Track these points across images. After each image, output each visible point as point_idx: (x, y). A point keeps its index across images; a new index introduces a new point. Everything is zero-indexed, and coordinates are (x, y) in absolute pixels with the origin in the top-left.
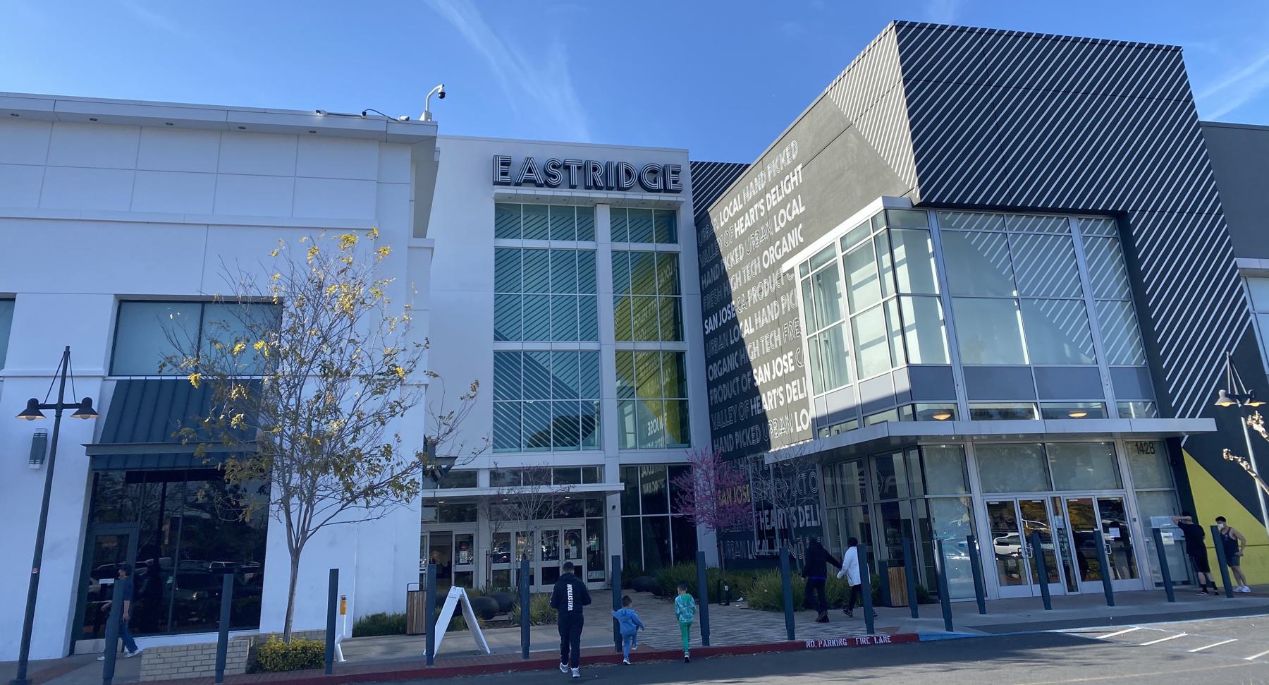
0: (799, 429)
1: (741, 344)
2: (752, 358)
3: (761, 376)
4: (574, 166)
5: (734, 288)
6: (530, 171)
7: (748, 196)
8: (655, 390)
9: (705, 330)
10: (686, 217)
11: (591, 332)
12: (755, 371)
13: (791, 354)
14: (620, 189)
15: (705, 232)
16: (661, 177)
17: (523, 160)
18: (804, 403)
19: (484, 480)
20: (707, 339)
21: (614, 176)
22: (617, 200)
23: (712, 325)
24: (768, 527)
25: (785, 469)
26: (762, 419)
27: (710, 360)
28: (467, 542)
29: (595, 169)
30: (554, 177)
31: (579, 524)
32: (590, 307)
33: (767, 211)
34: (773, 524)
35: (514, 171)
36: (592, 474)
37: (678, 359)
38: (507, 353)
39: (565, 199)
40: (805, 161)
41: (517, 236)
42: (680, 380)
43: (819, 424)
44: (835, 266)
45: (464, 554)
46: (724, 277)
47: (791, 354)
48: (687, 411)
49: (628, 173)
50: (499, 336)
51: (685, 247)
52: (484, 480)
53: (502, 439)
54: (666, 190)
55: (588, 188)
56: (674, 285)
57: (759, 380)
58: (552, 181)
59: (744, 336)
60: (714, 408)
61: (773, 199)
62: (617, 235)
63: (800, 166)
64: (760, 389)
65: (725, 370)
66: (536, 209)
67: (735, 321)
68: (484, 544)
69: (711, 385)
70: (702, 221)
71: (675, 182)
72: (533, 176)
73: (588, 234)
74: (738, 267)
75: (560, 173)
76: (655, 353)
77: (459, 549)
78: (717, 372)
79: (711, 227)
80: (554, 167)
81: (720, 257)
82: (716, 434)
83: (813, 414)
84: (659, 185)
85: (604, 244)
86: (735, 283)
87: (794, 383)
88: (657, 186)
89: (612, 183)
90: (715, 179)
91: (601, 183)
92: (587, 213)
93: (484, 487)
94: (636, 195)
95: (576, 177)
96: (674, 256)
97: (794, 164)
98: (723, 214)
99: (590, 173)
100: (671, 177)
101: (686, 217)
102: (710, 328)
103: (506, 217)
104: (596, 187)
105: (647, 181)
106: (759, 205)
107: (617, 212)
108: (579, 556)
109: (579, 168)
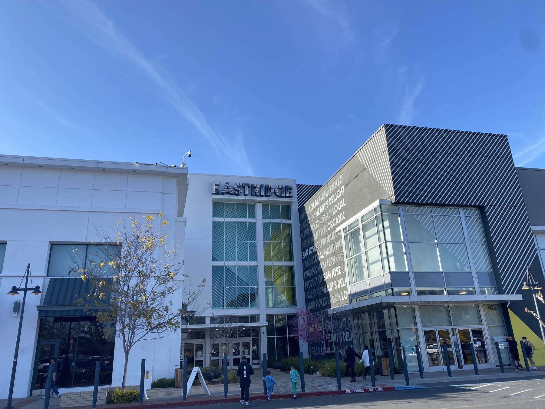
0: (343, 299)
1: (318, 263)
2: (323, 269)
3: (327, 276)
5: (315, 239)
6: (228, 188)
7: (321, 199)
8: (281, 282)
9: (303, 256)
10: (295, 208)
11: (254, 258)
12: (324, 274)
13: (340, 267)
15: (303, 214)
16: (284, 191)
17: (224, 184)
18: (345, 288)
19: (208, 321)
20: (304, 260)
21: (264, 191)
22: (265, 201)
24: (330, 341)
25: (337, 316)
26: (327, 295)
27: (305, 270)
28: (201, 348)
29: (255, 188)
31: (249, 340)
32: (254, 247)
35: (221, 188)
36: (254, 318)
39: (242, 200)
41: (222, 216)
42: (292, 278)
43: (352, 297)
44: (359, 229)
45: (199, 353)
46: (311, 234)
47: (340, 267)
49: (270, 189)
51: (294, 221)
52: (208, 321)
53: (216, 304)
54: (286, 197)
55: (252, 196)
56: (290, 237)
57: (326, 278)
58: (237, 192)
59: (319, 259)
60: (307, 290)
61: (332, 200)
62: (265, 216)
63: (343, 187)
66: (230, 204)
67: (316, 253)
69: (305, 280)
70: (302, 210)
71: (290, 193)
72: (229, 191)
75: (241, 189)
76: (281, 267)
77: (197, 351)
78: (308, 275)
79: (305, 213)
80: (238, 186)
81: (309, 225)
82: (308, 301)
85: (259, 220)
86: (316, 236)
87: (341, 280)
88: (282, 195)
89: (263, 194)
90: (307, 192)
91: (258, 193)
92: (252, 206)
93: (208, 324)
95: (248, 191)
96: (289, 225)
97: (341, 185)
98: (311, 207)
99: (253, 189)
100: (288, 191)
101: (295, 208)
102: (305, 256)
105: (278, 193)
106: (326, 203)
107: (265, 206)
109: (249, 187)
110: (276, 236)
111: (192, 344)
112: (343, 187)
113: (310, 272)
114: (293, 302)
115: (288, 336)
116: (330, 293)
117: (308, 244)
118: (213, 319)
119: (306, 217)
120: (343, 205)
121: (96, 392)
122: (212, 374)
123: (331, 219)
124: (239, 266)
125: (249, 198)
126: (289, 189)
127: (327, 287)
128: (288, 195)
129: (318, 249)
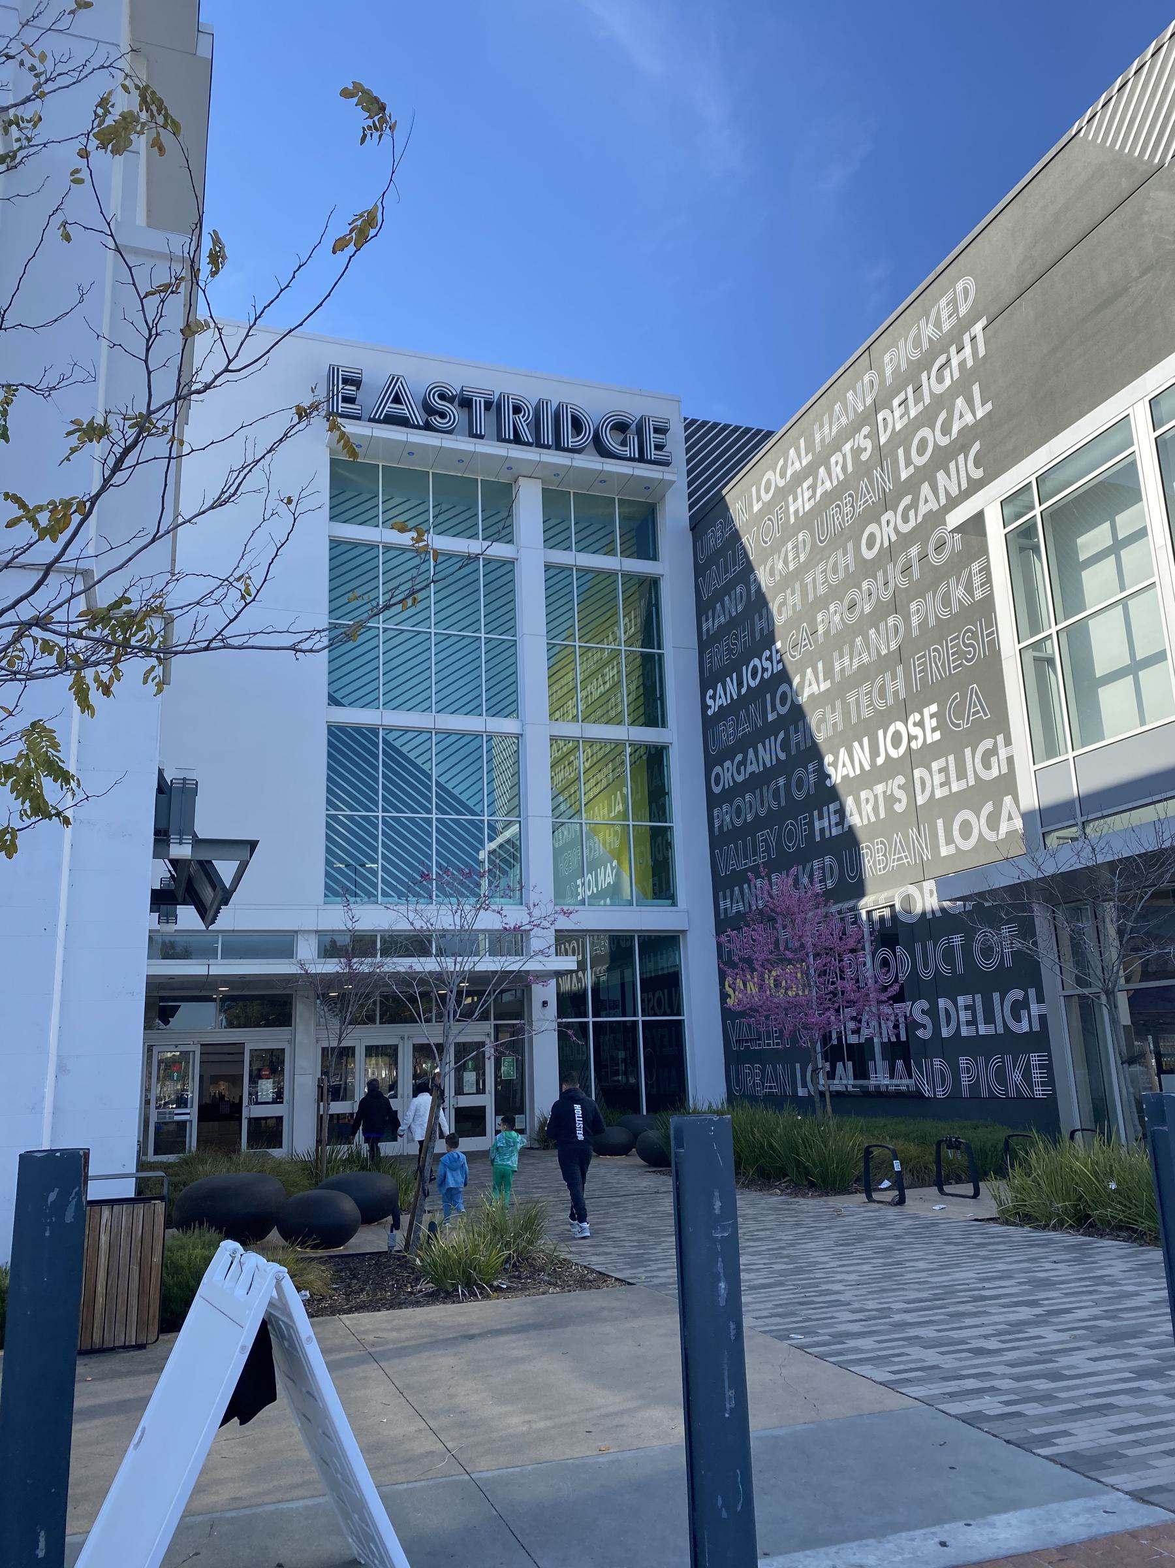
0: (945, 851)
1: (797, 714)
2: (820, 737)
3: (841, 767)
4: (479, 401)
5: (779, 620)
6: (397, 400)
7: (824, 432)
8: (609, 814)
9: (705, 707)
10: (675, 514)
11: (505, 700)
12: (828, 759)
13: (934, 708)
14: (558, 447)
15: (714, 538)
16: (631, 435)
17: (383, 380)
18: (1008, 783)
19: (307, 950)
20: (709, 723)
21: (556, 427)
22: (558, 472)
23: (726, 694)
24: (853, 1039)
25: (893, 933)
26: (847, 844)
27: (711, 761)
28: (272, 1064)
29: (517, 410)
30: (443, 415)
31: (479, 1032)
32: (505, 656)
33: (878, 448)
34: (865, 1032)
35: (368, 398)
36: (511, 940)
37: (654, 760)
38: (358, 729)
39: (461, 458)
40: (995, 309)
41: (371, 521)
42: (656, 798)
43: (1045, 820)
44: (1131, 468)
45: (267, 1088)
46: (759, 603)
47: (934, 708)
48: (669, 845)
49: (577, 424)
50: (333, 701)
51: (672, 566)
52: (307, 950)
53: (344, 882)
54: (642, 459)
55: (501, 439)
56: (650, 631)
57: (836, 776)
58: (436, 421)
59: (803, 699)
60: (718, 841)
61: (894, 419)
62: (554, 536)
63: (978, 327)
64: (841, 791)
65: (750, 769)
66: (406, 480)
67: (783, 677)
68: (304, 1074)
69: (713, 801)
70: (709, 515)
71: (659, 447)
72: (402, 410)
73: (502, 530)
74: (787, 581)
75: (452, 409)
76: (618, 744)
77: (255, 1078)
78: (728, 773)
79: (729, 521)
80: (442, 397)
81: (749, 568)
82: (722, 884)
83: (1029, 799)
84: (632, 450)
85: (529, 549)
86: (783, 609)
87: (935, 766)
88: (626, 451)
89: (548, 437)
90: (724, 451)
91: (527, 435)
92: (501, 497)
93: (309, 960)
94: (589, 462)
95: (484, 421)
96: (653, 584)
97: (964, 325)
98: (749, 500)
99: (509, 417)
100: (652, 438)
101: (675, 514)
102: (714, 707)
103: (352, 484)
104: (517, 440)
105: (611, 440)
106: (862, 440)
107: (552, 500)
108: (481, 1091)
109: (488, 405)
110: (598, 618)
111: (237, 1049)
112: (978, 327)
113: (743, 763)
114: (660, 883)
115: (591, 1019)
116: (861, 835)
117: (739, 648)
118: (330, 948)
119: (736, 536)
120: (965, 416)
121: (340, 1041)
122: (348, 1206)
123: (887, 503)
124: (449, 733)
125: (490, 448)
126: (657, 430)
127: (841, 812)
128: (653, 454)
129: (792, 659)
